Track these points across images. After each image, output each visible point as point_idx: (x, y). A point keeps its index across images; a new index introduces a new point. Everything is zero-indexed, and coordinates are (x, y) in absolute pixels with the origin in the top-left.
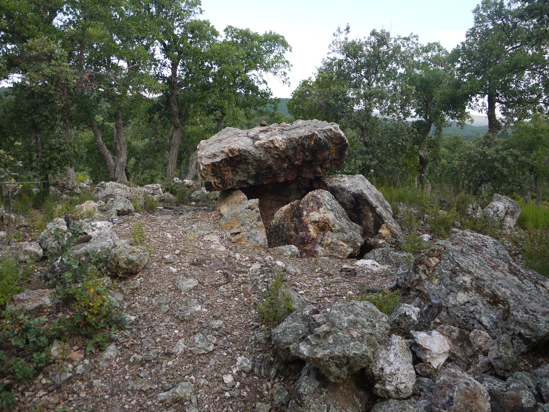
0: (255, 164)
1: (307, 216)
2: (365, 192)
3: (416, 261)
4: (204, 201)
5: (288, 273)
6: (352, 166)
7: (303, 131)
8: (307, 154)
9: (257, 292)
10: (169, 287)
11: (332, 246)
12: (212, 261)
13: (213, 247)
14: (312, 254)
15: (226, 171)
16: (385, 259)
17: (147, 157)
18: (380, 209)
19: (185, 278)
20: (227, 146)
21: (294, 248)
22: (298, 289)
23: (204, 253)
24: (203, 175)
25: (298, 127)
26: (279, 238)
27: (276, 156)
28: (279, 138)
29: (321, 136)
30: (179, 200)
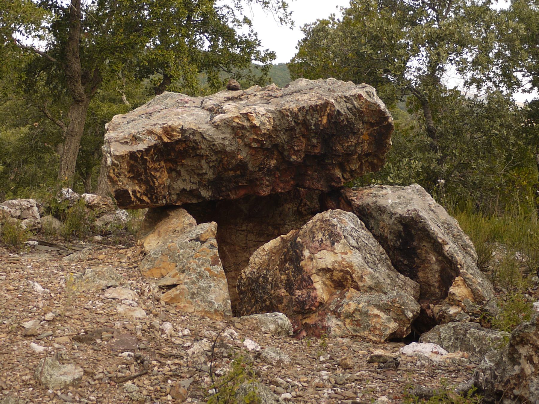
0: (214, 158)
1: (311, 259)
2: (423, 214)
3: (514, 337)
4: (118, 235)
5: (264, 361)
6: (403, 172)
7: (306, 97)
8: (315, 141)
9: (198, 393)
10: (24, 378)
11: (357, 316)
12: (114, 335)
13: (120, 309)
14: (318, 332)
15: (156, 170)
16: (460, 342)
17: (25, 162)
18: (450, 247)
19: (57, 363)
20: (160, 122)
21: (282, 318)
22: (279, 389)
23: (102, 321)
24: (112, 175)
25: (299, 91)
26: (257, 302)
27: (254, 145)
28: (261, 109)
29: (341, 107)
30: (72, 231)
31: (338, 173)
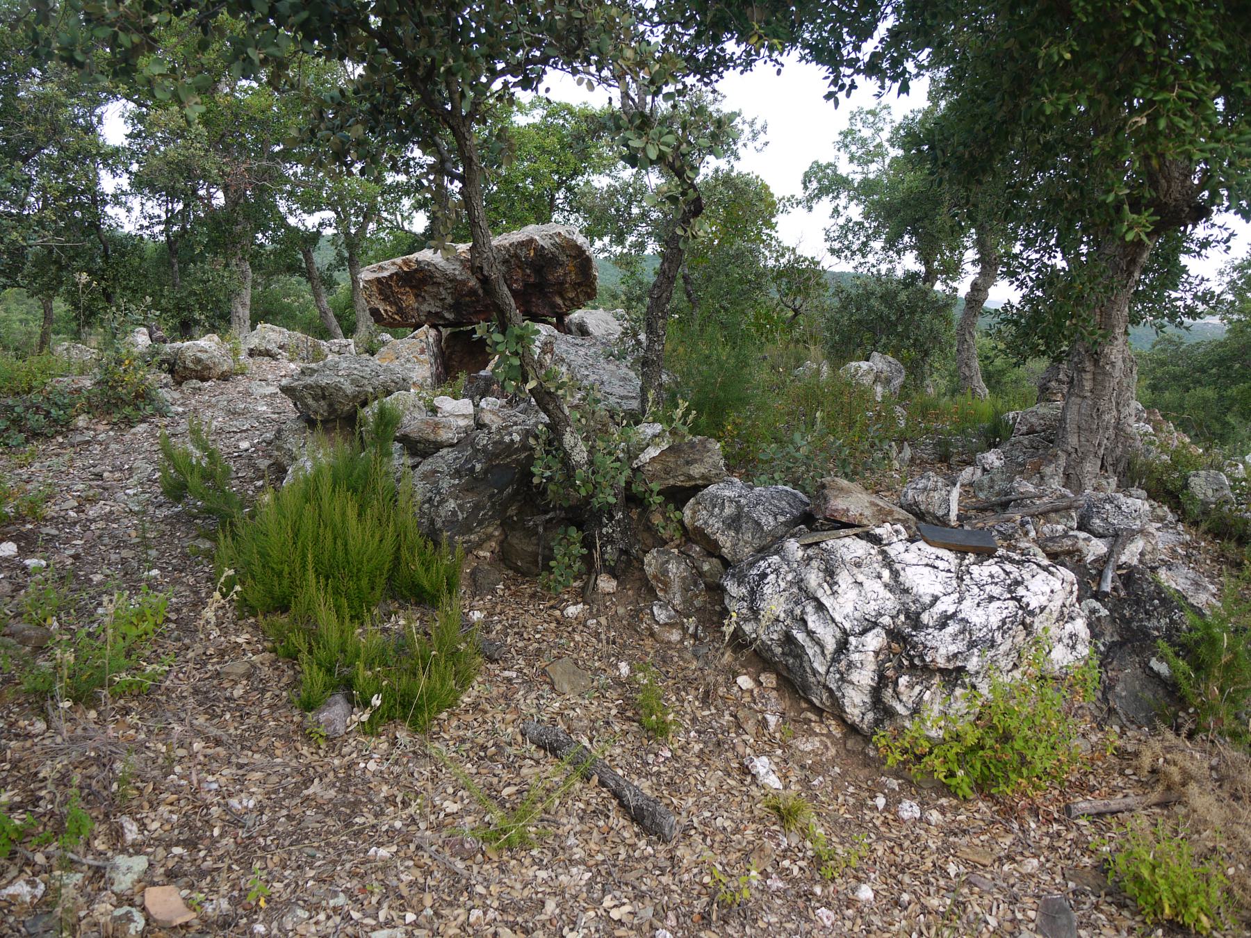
8: (528, 271)
15: (403, 294)
29: (546, 243)
31: (559, 301)
